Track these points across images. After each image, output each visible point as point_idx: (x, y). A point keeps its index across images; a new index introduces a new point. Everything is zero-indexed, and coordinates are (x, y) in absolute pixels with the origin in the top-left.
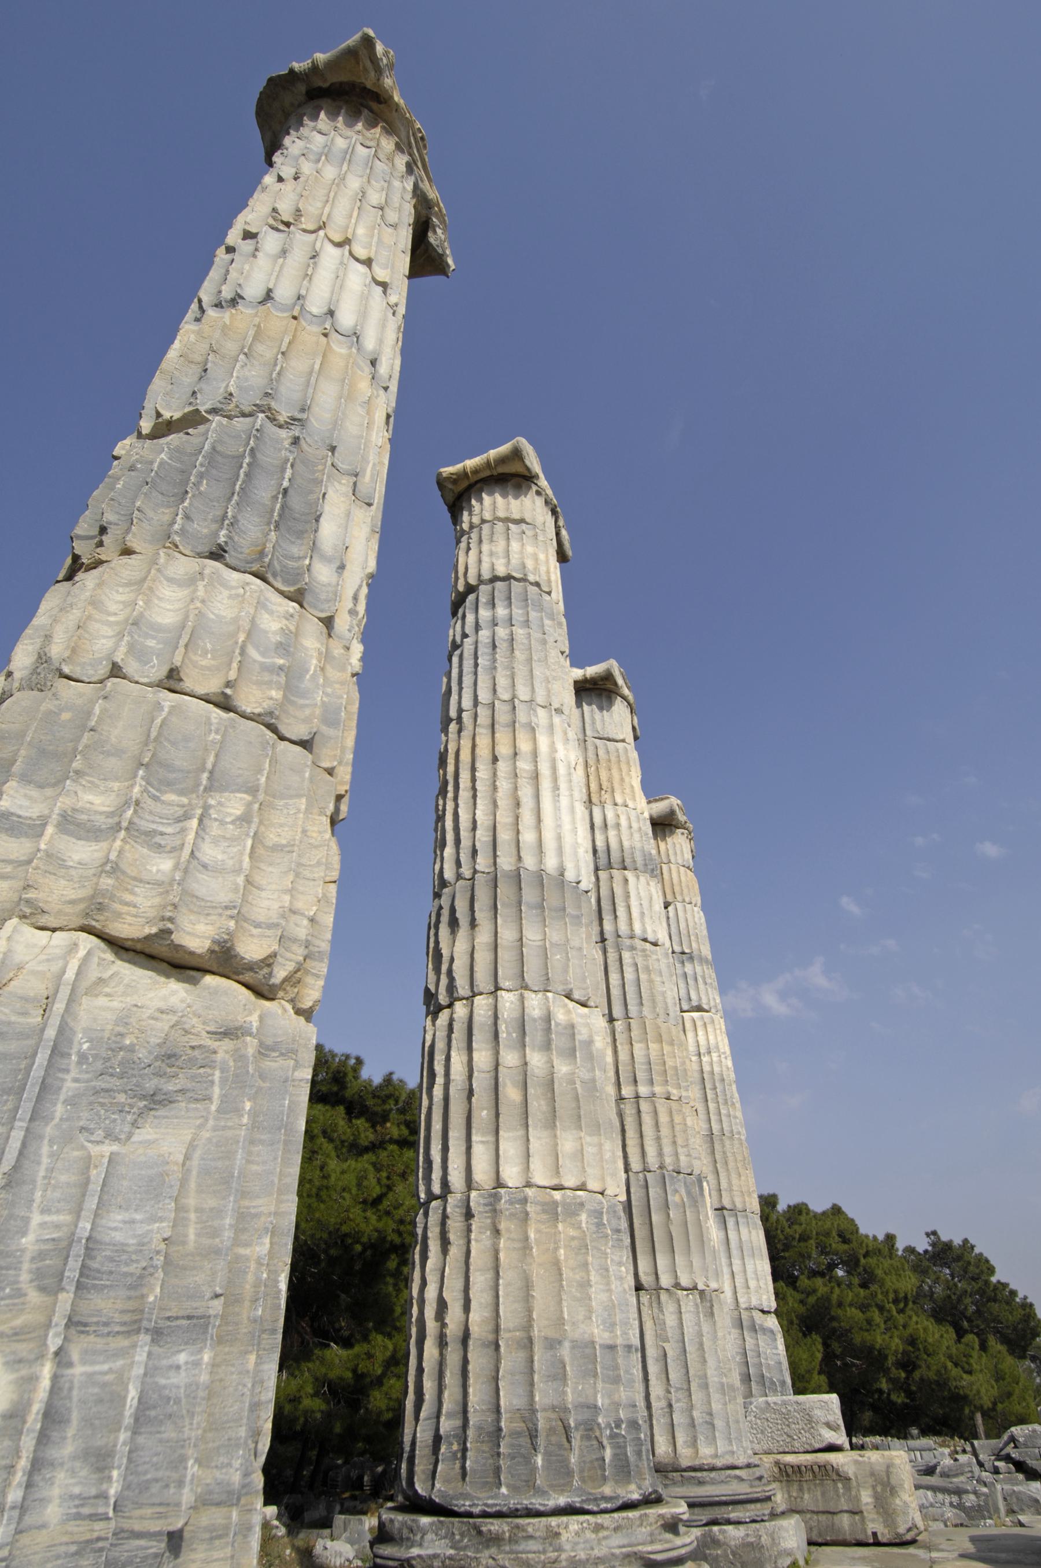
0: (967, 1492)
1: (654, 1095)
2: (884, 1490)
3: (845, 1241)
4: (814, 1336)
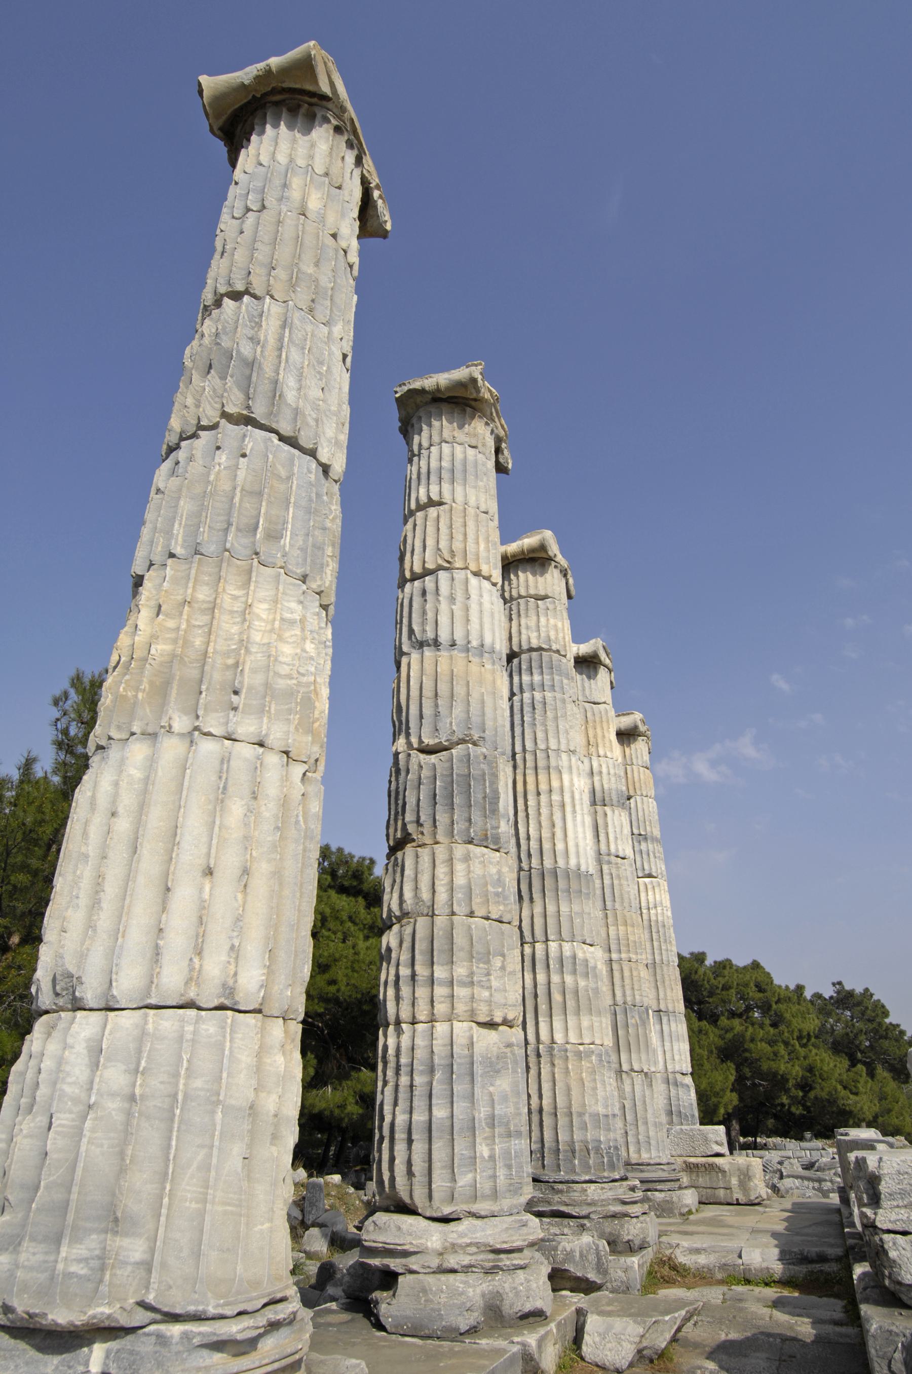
0: (825, 1180)
1: (621, 959)
2: (745, 1178)
3: (761, 990)
4: (729, 1064)
